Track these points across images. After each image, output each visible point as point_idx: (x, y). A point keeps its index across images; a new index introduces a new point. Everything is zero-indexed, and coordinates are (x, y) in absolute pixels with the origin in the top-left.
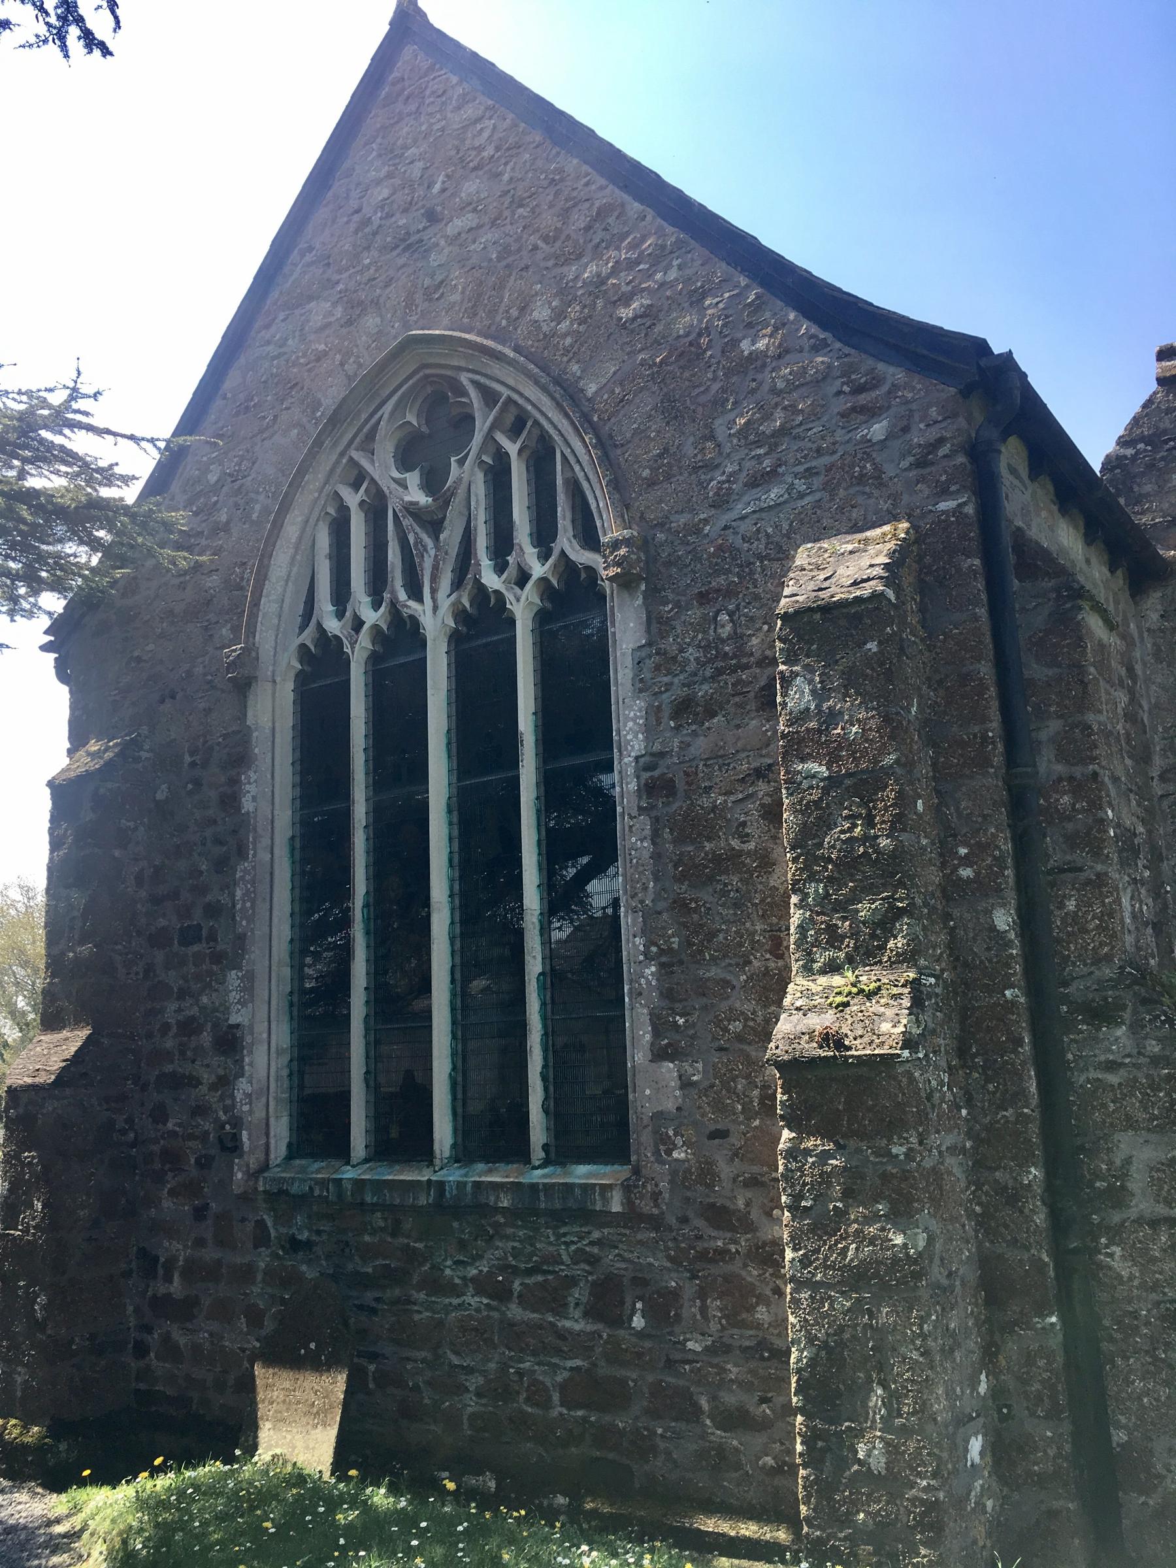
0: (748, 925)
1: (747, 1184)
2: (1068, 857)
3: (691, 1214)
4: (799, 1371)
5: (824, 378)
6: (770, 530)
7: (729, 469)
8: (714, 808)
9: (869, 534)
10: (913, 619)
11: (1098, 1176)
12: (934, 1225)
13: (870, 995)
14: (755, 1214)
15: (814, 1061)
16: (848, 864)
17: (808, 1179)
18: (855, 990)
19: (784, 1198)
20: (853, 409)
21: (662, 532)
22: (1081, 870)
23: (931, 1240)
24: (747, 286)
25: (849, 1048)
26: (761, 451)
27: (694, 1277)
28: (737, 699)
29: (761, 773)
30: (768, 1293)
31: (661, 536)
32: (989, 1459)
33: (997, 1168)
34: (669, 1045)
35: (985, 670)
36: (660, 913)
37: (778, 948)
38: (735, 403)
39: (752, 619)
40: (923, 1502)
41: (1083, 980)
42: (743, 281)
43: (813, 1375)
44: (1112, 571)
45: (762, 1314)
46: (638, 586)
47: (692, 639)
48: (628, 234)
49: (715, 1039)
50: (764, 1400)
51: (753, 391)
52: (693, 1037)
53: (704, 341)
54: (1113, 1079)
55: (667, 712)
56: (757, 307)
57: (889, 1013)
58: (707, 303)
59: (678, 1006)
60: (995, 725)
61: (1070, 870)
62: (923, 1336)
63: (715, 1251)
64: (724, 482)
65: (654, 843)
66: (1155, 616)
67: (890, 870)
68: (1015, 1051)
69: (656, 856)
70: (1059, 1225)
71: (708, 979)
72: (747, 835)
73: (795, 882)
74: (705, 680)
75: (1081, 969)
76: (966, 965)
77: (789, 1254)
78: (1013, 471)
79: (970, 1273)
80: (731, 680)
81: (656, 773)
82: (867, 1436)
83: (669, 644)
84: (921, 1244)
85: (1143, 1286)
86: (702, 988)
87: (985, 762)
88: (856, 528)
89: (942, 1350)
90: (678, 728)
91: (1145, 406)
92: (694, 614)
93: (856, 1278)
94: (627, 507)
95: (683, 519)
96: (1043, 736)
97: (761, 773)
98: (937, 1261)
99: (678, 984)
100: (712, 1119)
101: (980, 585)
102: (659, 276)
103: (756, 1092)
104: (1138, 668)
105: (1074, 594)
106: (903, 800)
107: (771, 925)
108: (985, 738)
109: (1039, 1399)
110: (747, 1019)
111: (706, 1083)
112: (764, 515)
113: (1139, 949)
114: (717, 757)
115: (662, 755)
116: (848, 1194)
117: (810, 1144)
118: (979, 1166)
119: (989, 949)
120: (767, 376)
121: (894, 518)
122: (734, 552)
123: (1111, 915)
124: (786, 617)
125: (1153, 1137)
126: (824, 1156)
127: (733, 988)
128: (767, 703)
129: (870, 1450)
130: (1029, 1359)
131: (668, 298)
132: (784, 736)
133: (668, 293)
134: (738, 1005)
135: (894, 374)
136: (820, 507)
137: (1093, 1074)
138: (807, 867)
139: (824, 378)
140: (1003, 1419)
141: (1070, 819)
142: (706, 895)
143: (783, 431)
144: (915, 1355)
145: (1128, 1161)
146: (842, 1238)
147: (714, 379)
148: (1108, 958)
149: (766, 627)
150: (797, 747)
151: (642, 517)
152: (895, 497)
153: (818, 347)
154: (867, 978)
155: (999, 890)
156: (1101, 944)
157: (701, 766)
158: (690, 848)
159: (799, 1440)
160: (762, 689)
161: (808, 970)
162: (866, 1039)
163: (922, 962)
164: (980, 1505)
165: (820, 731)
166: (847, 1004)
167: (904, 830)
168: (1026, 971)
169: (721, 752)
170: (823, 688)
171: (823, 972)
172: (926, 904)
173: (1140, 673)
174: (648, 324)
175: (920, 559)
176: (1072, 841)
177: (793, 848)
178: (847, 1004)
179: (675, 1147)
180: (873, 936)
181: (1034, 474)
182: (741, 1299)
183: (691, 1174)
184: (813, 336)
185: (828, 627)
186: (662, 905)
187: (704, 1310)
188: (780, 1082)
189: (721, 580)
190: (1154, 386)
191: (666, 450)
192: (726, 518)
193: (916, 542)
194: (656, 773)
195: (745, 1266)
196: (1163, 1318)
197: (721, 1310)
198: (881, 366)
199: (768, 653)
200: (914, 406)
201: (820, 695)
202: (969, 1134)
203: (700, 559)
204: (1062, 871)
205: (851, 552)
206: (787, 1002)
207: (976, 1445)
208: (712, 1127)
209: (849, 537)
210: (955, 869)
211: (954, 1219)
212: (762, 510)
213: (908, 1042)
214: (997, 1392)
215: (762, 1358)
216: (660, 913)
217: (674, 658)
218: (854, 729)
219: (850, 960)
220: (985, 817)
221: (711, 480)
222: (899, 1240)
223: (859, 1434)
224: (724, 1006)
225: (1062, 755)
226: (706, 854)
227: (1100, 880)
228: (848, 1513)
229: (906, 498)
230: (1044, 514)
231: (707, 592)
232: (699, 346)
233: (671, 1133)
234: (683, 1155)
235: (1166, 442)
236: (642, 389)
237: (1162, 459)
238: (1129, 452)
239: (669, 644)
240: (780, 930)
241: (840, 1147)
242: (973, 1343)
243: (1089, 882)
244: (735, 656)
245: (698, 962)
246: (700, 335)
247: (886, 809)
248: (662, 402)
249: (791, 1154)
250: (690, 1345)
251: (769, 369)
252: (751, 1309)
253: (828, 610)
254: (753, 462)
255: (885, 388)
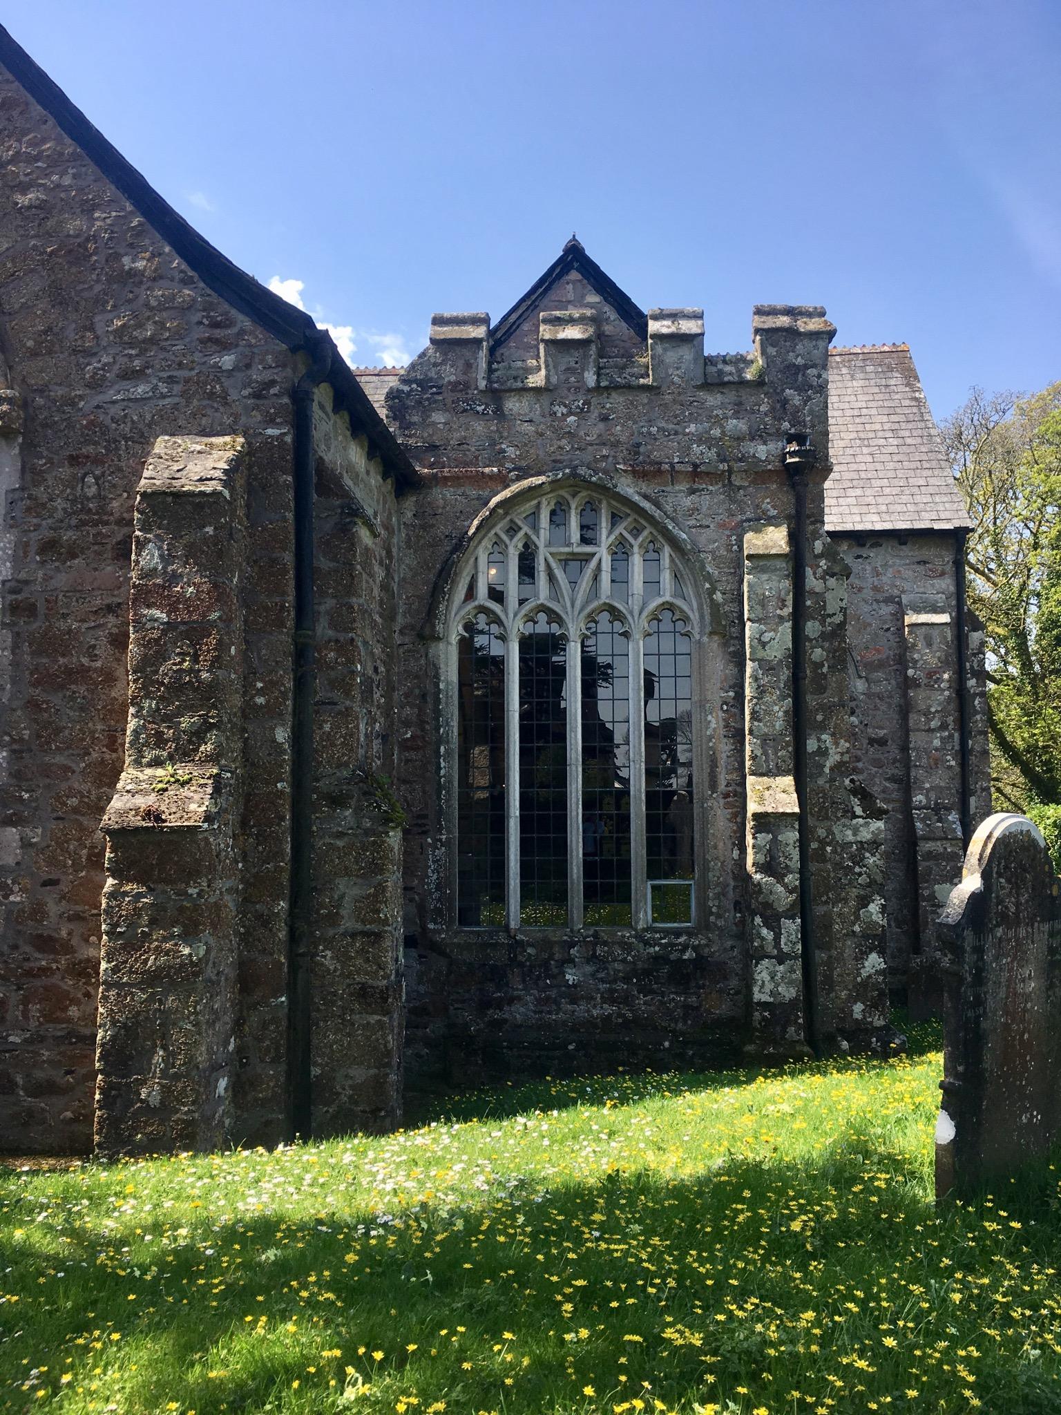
0: (90, 725)
1: (70, 919)
2: (330, 695)
3: (21, 942)
4: (103, 1045)
5: (189, 308)
6: (135, 418)
7: (105, 359)
8: (70, 631)
9: (214, 440)
10: (240, 512)
11: (322, 906)
12: (211, 941)
13: (183, 784)
14: (75, 942)
15: (137, 830)
16: (177, 688)
17: (124, 913)
18: (172, 780)
19: (104, 927)
20: (210, 339)
21: (41, 397)
22: (335, 704)
23: (208, 951)
24: (131, 212)
25: (165, 821)
26: (133, 352)
27: (19, 988)
28: (96, 547)
29: (110, 609)
30: (80, 995)
31: (40, 401)
32: (230, 1093)
33: (259, 902)
34: (14, 814)
35: (288, 558)
36: (14, 710)
37: (114, 743)
38: (114, 306)
39: (114, 486)
40: (184, 1121)
41: (328, 777)
42: (129, 207)
43: (113, 1047)
44: (385, 477)
45: (73, 1011)
46: (15, 438)
47: (62, 492)
48: (29, 131)
49: (53, 810)
50: (68, 1072)
51: (129, 301)
52: (36, 809)
53: (91, 246)
54: (340, 843)
55: (33, 548)
56: (139, 232)
57: (197, 797)
58: (96, 215)
59: (24, 784)
60: (291, 598)
61: (329, 703)
62: (196, 1013)
63: (39, 969)
64: (100, 369)
65: (13, 653)
66: (409, 514)
67: (207, 695)
68: (279, 825)
69: (15, 664)
70: (293, 937)
71: (53, 765)
72: (96, 655)
73: (134, 698)
74: (70, 527)
75: (330, 770)
76: (253, 764)
77: (103, 965)
78: (322, 407)
79: (232, 974)
80: (93, 531)
81: (19, 597)
82: (149, 1083)
83: (40, 492)
84: (202, 953)
85: (342, 974)
86: (46, 771)
87: (283, 625)
88: (204, 433)
89: (208, 1022)
90: (43, 562)
91: (420, 357)
92: (65, 472)
93: (152, 979)
94: (11, 368)
95: (60, 391)
96: (322, 608)
97: (110, 609)
98: (210, 964)
99: (26, 767)
100: (45, 872)
101: (290, 495)
102: (55, 178)
103: (85, 851)
104: (394, 550)
105: (353, 511)
106: (221, 646)
107: (109, 726)
108: (283, 606)
109: (268, 1049)
110: (83, 796)
111: (44, 844)
112: (131, 404)
113: (367, 758)
114: (75, 591)
115: (26, 582)
116: (153, 922)
117: (128, 888)
118: (246, 901)
119: (270, 754)
120: (143, 293)
121: (232, 431)
122: (104, 430)
123: (351, 736)
124: (144, 495)
125: (359, 881)
126: (139, 896)
127: (74, 772)
128: (122, 553)
129: (150, 1093)
130: (264, 1025)
131: (62, 200)
132: (135, 586)
133: (63, 195)
134: (76, 785)
135: (243, 321)
136: (177, 410)
137: (328, 840)
138: (144, 687)
139: (189, 308)
140: (243, 1066)
141: (333, 669)
142: (56, 699)
143: (152, 341)
144: (189, 1027)
145: (342, 897)
146: (145, 952)
147: (98, 281)
148: (346, 764)
149: (125, 495)
150: (144, 596)
151: (23, 380)
152: (236, 417)
153: (187, 282)
154: (183, 772)
155: (281, 714)
156: (344, 754)
157: (60, 597)
158: (44, 661)
159: (98, 1092)
160: (118, 543)
161: (138, 763)
162: (178, 815)
163: (223, 762)
164: (221, 1122)
165: (164, 588)
166: (166, 790)
167: (220, 668)
168: (293, 771)
169: (80, 588)
170: (169, 555)
171: (149, 765)
172: (230, 721)
173: (395, 554)
174: (42, 216)
175: (250, 467)
176: (333, 684)
177: (135, 672)
178: (166, 790)
179: (12, 892)
180: (190, 742)
181: (336, 409)
182: (57, 1002)
183: (24, 912)
184: (182, 271)
185: (173, 507)
186: (15, 704)
187: (25, 1014)
188: (109, 844)
189: (91, 449)
190: (428, 343)
191: (50, 329)
192: (99, 399)
193: (248, 454)
194: (19, 597)
195: (63, 978)
196: (351, 995)
197: (40, 1011)
198: (234, 312)
199: (125, 515)
200: (256, 350)
201: (166, 559)
202: (242, 881)
203: (74, 427)
204: (324, 703)
205: (199, 452)
206: (119, 786)
207: (223, 1083)
208: (46, 877)
209: (198, 439)
210: (253, 697)
211: (226, 937)
212: (130, 400)
213: (208, 818)
214: (239, 1050)
215: (71, 1044)
216: (14, 710)
217: (44, 505)
218: (190, 590)
219: (171, 757)
220: (277, 662)
221: (89, 364)
222: (187, 951)
223: (143, 1083)
224: (64, 786)
225: (333, 625)
226: (60, 667)
227: (347, 713)
228: (130, 1135)
229: (243, 419)
230: (340, 438)
231: (78, 457)
232: (86, 249)
233: (9, 882)
234: (18, 899)
235: (432, 387)
236: (32, 271)
237: (428, 399)
238: (406, 388)
239: (40, 492)
240: (116, 731)
241: (150, 890)
242: (228, 1018)
243: (340, 713)
244: (97, 513)
245: (45, 751)
246: (88, 240)
247: (208, 651)
248: (50, 287)
249: (112, 895)
250: (11, 1039)
251: (145, 287)
252: (65, 1009)
253: (179, 496)
254: (126, 359)
255: (235, 330)
